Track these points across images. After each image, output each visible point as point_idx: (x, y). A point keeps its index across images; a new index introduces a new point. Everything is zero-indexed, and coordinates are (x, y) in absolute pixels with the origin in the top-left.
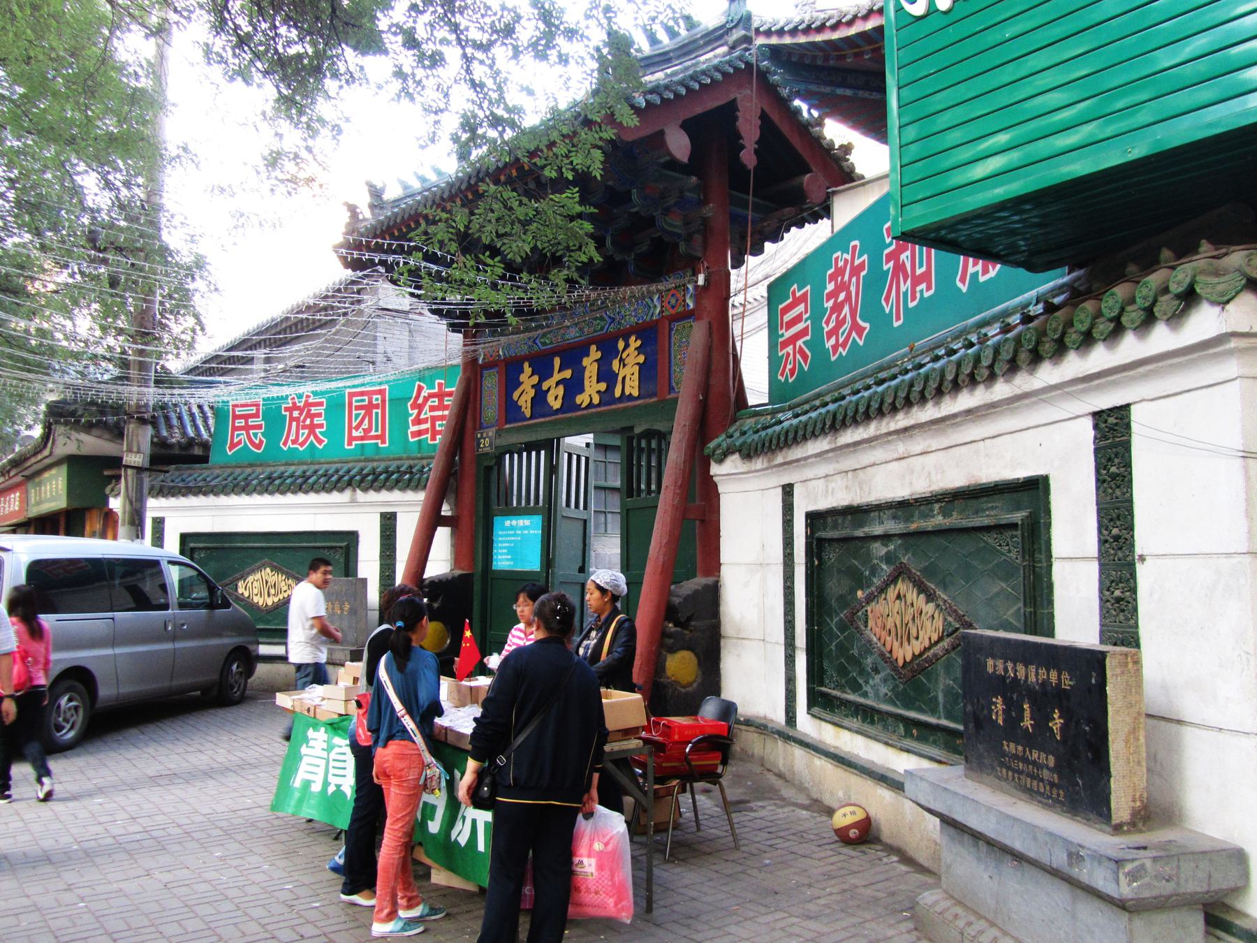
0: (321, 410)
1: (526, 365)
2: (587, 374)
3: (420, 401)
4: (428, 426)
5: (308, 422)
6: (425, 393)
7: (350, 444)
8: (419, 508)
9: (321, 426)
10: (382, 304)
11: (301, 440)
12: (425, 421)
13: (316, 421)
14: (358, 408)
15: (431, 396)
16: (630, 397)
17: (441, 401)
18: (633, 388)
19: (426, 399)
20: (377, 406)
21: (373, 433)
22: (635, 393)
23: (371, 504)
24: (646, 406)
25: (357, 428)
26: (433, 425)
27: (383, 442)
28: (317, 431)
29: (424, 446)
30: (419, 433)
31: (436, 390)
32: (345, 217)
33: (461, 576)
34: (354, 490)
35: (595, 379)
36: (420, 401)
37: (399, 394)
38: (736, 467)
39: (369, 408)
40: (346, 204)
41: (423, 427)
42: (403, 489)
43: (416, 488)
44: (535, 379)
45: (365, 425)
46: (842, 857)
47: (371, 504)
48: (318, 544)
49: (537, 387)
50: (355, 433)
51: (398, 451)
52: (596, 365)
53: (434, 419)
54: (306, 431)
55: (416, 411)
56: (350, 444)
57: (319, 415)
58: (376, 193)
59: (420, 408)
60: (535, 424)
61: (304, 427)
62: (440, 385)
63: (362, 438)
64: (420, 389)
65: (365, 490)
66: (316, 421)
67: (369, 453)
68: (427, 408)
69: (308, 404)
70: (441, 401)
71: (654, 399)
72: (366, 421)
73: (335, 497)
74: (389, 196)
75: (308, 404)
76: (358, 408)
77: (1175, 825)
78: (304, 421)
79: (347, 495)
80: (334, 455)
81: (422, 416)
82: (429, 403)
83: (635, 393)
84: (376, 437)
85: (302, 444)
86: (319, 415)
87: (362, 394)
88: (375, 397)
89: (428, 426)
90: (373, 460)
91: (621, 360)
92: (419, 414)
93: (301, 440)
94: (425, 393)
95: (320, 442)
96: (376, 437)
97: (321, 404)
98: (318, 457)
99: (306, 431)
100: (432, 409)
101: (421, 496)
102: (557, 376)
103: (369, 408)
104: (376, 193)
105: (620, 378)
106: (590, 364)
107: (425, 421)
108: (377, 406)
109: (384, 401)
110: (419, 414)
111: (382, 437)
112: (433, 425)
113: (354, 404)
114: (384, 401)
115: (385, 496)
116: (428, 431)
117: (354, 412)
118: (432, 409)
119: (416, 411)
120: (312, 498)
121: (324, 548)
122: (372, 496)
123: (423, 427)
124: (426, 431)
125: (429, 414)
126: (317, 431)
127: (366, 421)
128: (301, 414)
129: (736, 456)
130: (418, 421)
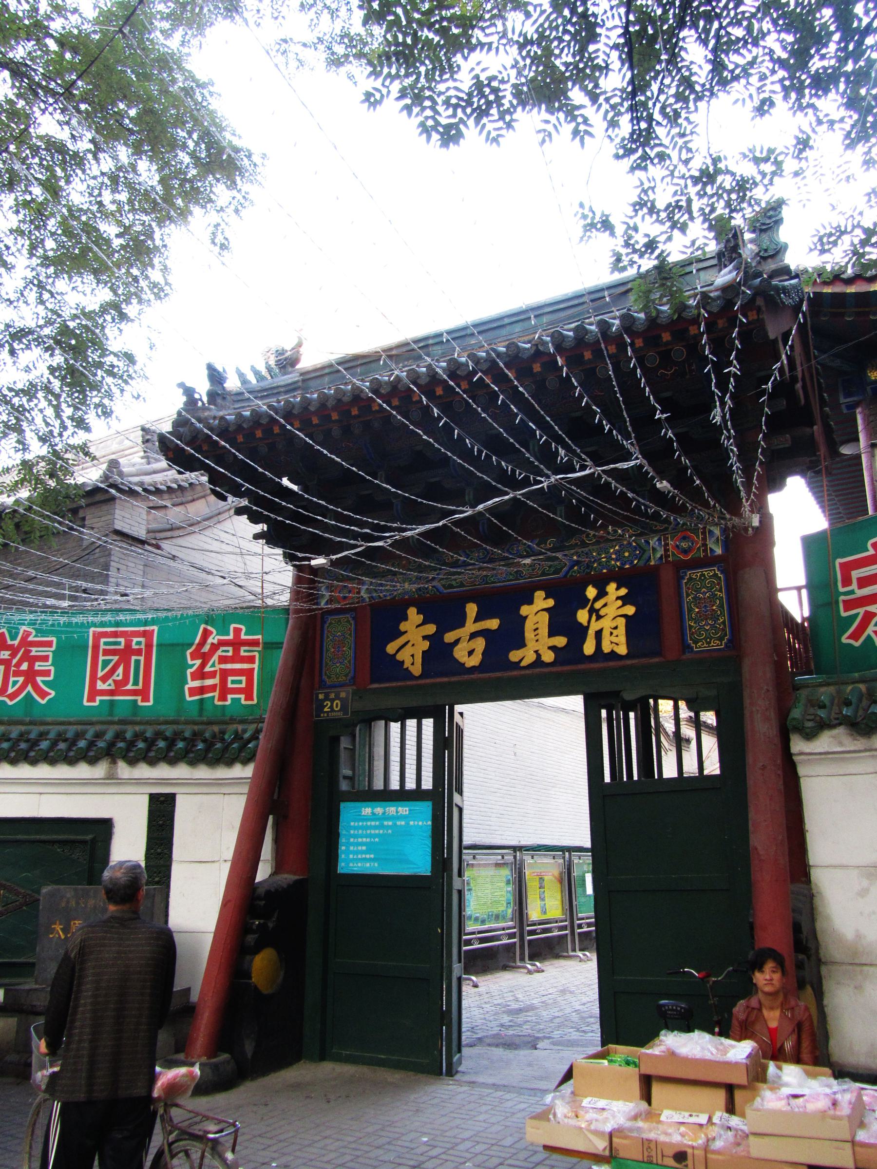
0: (48, 651)
1: (412, 612)
2: (529, 626)
3: (206, 648)
4: (215, 681)
5: (25, 666)
6: (213, 639)
7: (91, 699)
8: (246, 789)
9: (47, 673)
10: (118, 526)
11: (10, 690)
12: (212, 675)
13: (38, 666)
14: (106, 652)
15: (222, 643)
16: (613, 655)
17: (236, 651)
18: (617, 642)
19: (215, 647)
20: (138, 652)
21: (130, 687)
22: (622, 650)
23: (139, 782)
24: (559, 675)
25: (104, 679)
26: (224, 681)
27: (146, 699)
28: (39, 679)
29: (208, 706)
30: (202, 690)
31: (231, 637)
32: (179, 401)
33: (297, 882)
34: (114, 762)
35: (544, 630)
36: (206, 648)
37: (169, 639)
38: (841, 744)
39: (126, 654)
40: (181, 385)
41: (209, 682)
42: (193, 763)
43: (245, 762)
44: (431, 629)
45: (119, 674)
46: (325, 1159)
47: (139, 782)
48: (43, 837)
49: (435, 640)
50: (100, 686)
51: (168, 711)
52: (546, 616)
53: (225, 674)
54: (21, 679)
55: (198, 662)
56: (91, 699)
57: (45, 659)
58: (216, 376)
59: (205, 658)
60: (434, 685)
61: (17, 674)
62: (237, 631)
63: (111, 693)
64: (206, 634)
65: (132, 762)
66: (38, 666)
67: (121, 713)
68: (215, 658)
69: (25, 642)
70: (236, 651)
71: (656, 660)
72: (120, 670)
73: (83, 771)
74: (232, 384)
75: (25, 642)
76: (106, 652)
77: (451, 1072)
78: (19, 664)
79: (100, 770)
80: (62, 713)
81: (208, 669)
82: (219, 653)
83: (622, 650)
84: (134, 693)
85: (12, 697)
86: (45, 659)
87: (115, 634)
88: (135, 640)
89: (215, 681)
90: (21, 723)
91: (592, 611)
92: (203, 665)
93: (10, 690)
94: (213, 639)
95: (43, 694)
96: (134, 693)
97: (49, 644)
98: (37, 714)
99: (21, 679)
100: (223, 660)
101: (245, 772)
102: (471, 626)
103: (126, 654)
104: (216, 376)
105: (591, 632)
106: (537, 612)
107: (212, 675)
108: (138, 652)
109: (149, 646)
110: (203, 665)
111: (144, 693)
112: (224, 681)
113: (102, 647)
114: (149, 646)
115: (163, 771)
116: (247, 687)
117: (101, 658)
118: (223, 660)
119: (198, 662)
120: (43, 771)
121: (53, 842)
122: (143, 771)
123: (209, 682)
124: (213, 688)
125: (218, 667)
126: (39, 679)
127: (120, 670)
128: (13, 655)
129: (840, 731)
130: (200, 674)
